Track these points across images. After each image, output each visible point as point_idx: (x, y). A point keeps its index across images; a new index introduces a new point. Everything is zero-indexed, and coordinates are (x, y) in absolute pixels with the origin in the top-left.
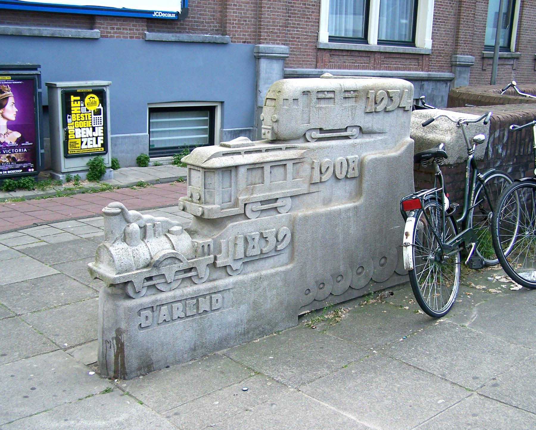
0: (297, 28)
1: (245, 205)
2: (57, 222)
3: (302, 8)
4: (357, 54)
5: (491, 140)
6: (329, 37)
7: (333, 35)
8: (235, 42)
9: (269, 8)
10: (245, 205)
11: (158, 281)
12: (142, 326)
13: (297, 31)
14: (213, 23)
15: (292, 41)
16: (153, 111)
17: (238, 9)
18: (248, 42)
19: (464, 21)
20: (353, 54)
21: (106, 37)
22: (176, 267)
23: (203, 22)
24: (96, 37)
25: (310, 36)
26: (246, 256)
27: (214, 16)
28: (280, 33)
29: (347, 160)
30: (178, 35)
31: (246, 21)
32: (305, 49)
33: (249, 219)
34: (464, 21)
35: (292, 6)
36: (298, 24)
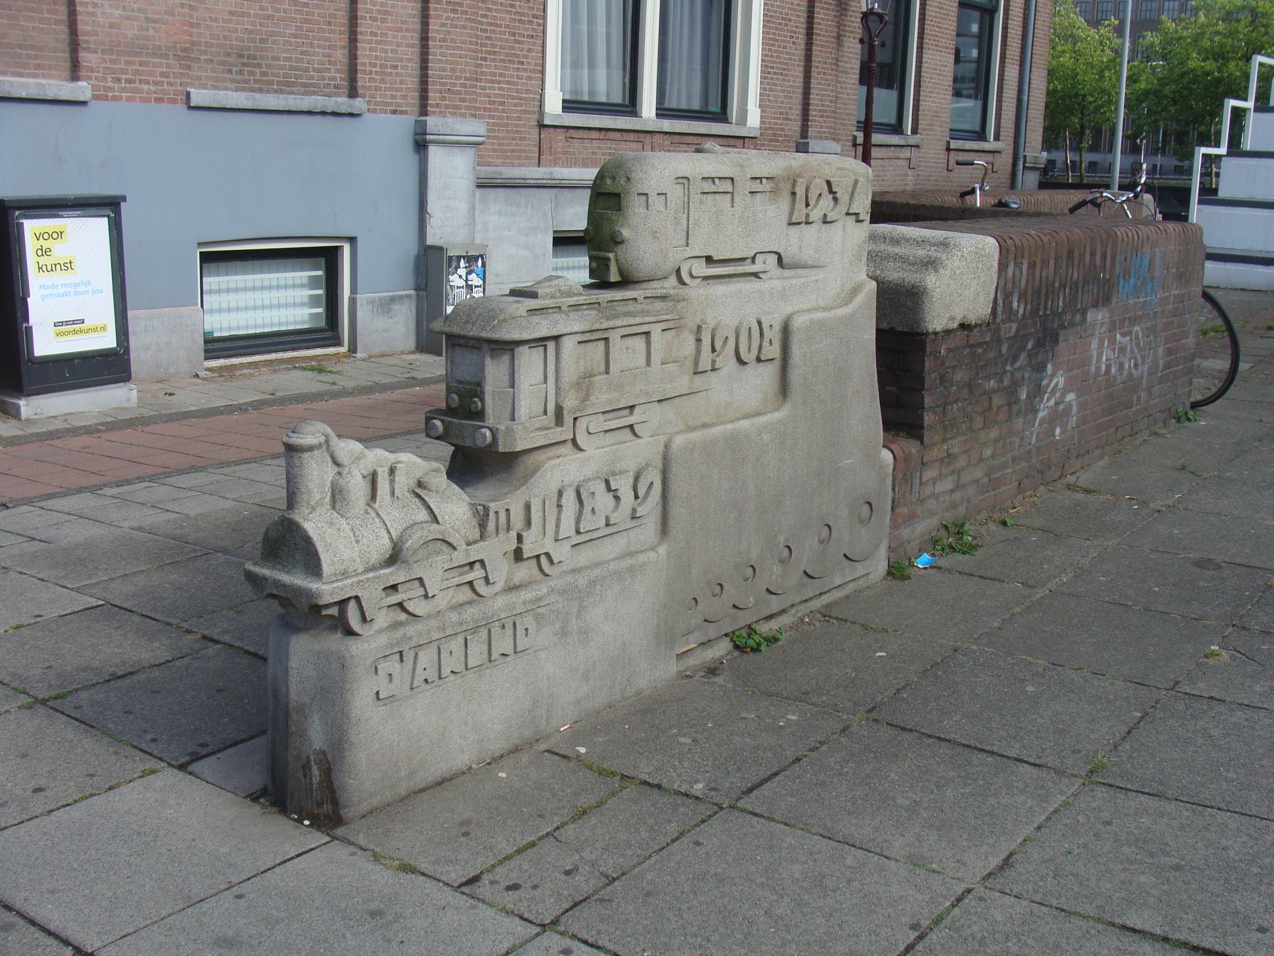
0: (499, 82)
1: (575, 419)
2: (51, 496)
3: (507, 41)
4: (618, 135)
5: (1002, 282)
6: (564, 101)
7: (568, 97)
8: (375, 111)
9: (444, 40)
10: (575, 419)
11: (410, 594)
12: (381, 697)
13: (501, 89)
14: (329, 70)
15: (490, 110)
16: (207, 258)
17: (379, 42)
18: (401, 113)
19: (819, 73)
20: (611, 135)
21: (106, 98)
22: (443, 559)
23: (307, 70)
24: (82, 99)
25: (525, 99)
26: (578, 532)
27: (329, 56)
28: (467, 93)
29: (759, 323)
30: (258, 96)
31: (396, 67)
32: (517, 126)
33: (582, 450)
34: (819, 73)
35: (488, 38)
36: (501, 75)
